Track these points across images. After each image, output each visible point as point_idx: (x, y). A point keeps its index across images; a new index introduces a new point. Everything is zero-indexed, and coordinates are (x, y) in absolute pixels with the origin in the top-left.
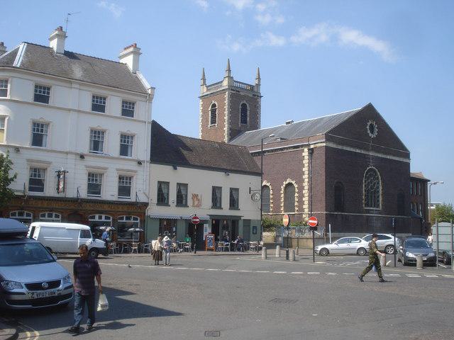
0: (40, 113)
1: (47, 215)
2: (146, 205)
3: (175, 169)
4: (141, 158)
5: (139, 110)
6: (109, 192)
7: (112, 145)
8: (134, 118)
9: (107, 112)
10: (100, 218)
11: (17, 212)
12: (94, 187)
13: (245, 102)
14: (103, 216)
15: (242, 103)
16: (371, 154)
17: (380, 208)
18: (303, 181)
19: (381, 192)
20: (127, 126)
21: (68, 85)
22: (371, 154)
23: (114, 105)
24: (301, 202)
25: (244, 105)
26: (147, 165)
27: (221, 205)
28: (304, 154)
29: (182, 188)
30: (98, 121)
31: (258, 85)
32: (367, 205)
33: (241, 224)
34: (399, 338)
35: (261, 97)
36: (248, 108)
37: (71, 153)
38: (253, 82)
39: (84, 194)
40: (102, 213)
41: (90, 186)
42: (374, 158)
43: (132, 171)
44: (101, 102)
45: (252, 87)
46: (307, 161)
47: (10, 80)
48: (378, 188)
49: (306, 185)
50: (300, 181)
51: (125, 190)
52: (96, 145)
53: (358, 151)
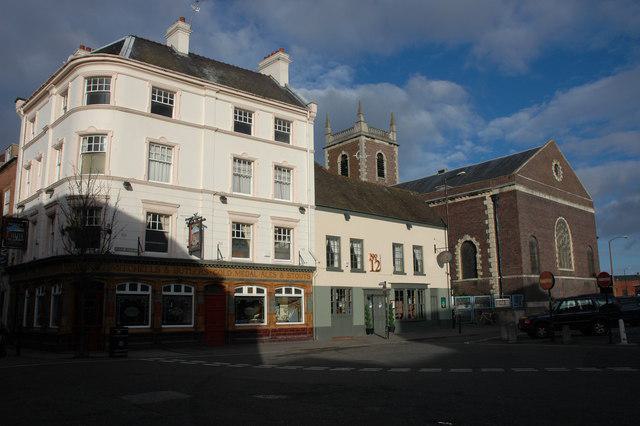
0: (159, 128)
2: (312, 269)
3: (347, 218)
4: (304, 202)
9: (112, 103)
12: (240, 245)
13: (380, 151)
14: (255, 288)
18: (487, 236)
24: (487, 265)
26: (311, 212)
27: (422, 269)
28: (485, 202)
29: (355, 245)
30: (242, 145)
32: (561, 266)
33: (427, 294)
36: (385, 158)
37: (208, 192)
39: (227, 256)
40: (253, 284)
41: (235, 243)
43: (292, 220)
44: (245, 120)
48: (568, 243)
49: (492, 241)
50: (483, 238)
51: (282, 251)
53: (547, 197)
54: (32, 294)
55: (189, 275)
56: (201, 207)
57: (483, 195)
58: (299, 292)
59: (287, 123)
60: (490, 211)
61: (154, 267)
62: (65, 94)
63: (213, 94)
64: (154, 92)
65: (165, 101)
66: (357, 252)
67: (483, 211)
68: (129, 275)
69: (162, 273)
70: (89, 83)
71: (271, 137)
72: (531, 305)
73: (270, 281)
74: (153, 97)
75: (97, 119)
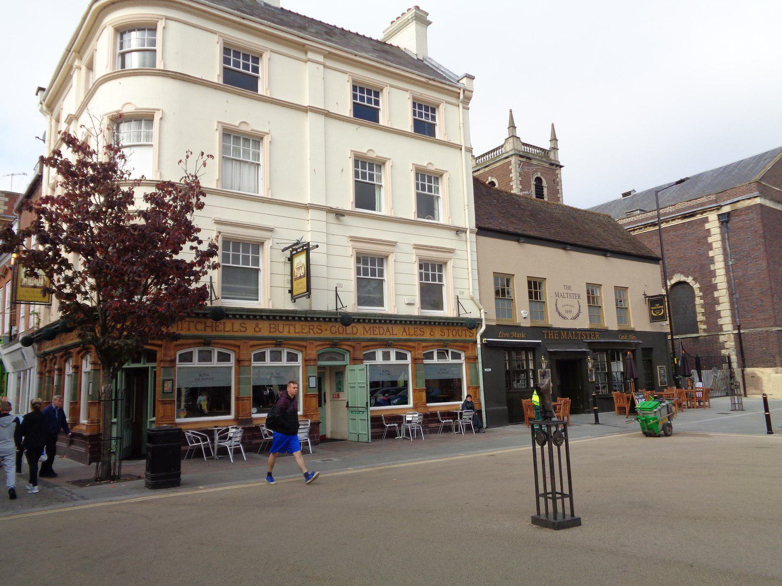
0: (239, 111)
5: (447, 120)
6: (401, 296)
7: (397, 194)
10: (386, 356)
11: (196, 352)
12: (370, 285)
13: (539, 175)
15: (535, 177)
18: (713, 274)
20: (424, 154)
21: (302, 56)
23: (397, 108)
25: (538, 180)
28: (707, 226)
30: (366, 140)
31: (555, 149)
35: (561, 167)
36: (544, 183)
38: (547, 146)
39: (350, 304)
46: (718, 237)
47: (160, 25)
51: (431, 294)
52: (366, 196)
54: (77, 368)
55: (292, 335)
56: (310, 227)
57: (705, 215)
58: (224, 357)
59: (433, 109)
60: (715, 238)
61: (237, 324)
62: (90, 67)
63: (320, 58)
67: (706, 237)
68: (193, 337)
69: (250, 332)
71: (409, 127)
73: (415, 341)
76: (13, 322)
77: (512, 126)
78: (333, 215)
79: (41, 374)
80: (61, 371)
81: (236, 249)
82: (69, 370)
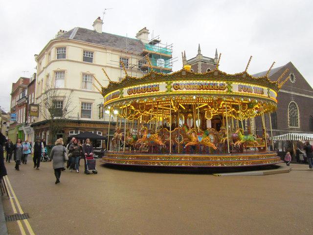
0: (87, 68)
1: (74, 132)
8: (66, 58)
16: (292, 93)
17: (299, 127)
19: (299, 117)
22: (292, 93)
32: (291, 125)
34: (303, 234)
38: (213, 57)
42: (294, 96)
45: (212, 60)
48: (297, 114)
54: (45, 134)
63: (111, 52)
64: (84, 52)
65: (89, 56)
66: (105, 145)
69: (88, 127)
70: (58, 50)
72: (289, 153)
74: (84, 55)
75: (60, 65)
76: (26, 119)
77: (199, 50)
78: (77, 124)
79: (35, 135)
80: (41, 134)
81: (85, 105)
82: (43, 134)
